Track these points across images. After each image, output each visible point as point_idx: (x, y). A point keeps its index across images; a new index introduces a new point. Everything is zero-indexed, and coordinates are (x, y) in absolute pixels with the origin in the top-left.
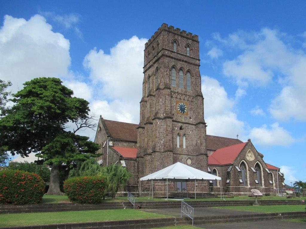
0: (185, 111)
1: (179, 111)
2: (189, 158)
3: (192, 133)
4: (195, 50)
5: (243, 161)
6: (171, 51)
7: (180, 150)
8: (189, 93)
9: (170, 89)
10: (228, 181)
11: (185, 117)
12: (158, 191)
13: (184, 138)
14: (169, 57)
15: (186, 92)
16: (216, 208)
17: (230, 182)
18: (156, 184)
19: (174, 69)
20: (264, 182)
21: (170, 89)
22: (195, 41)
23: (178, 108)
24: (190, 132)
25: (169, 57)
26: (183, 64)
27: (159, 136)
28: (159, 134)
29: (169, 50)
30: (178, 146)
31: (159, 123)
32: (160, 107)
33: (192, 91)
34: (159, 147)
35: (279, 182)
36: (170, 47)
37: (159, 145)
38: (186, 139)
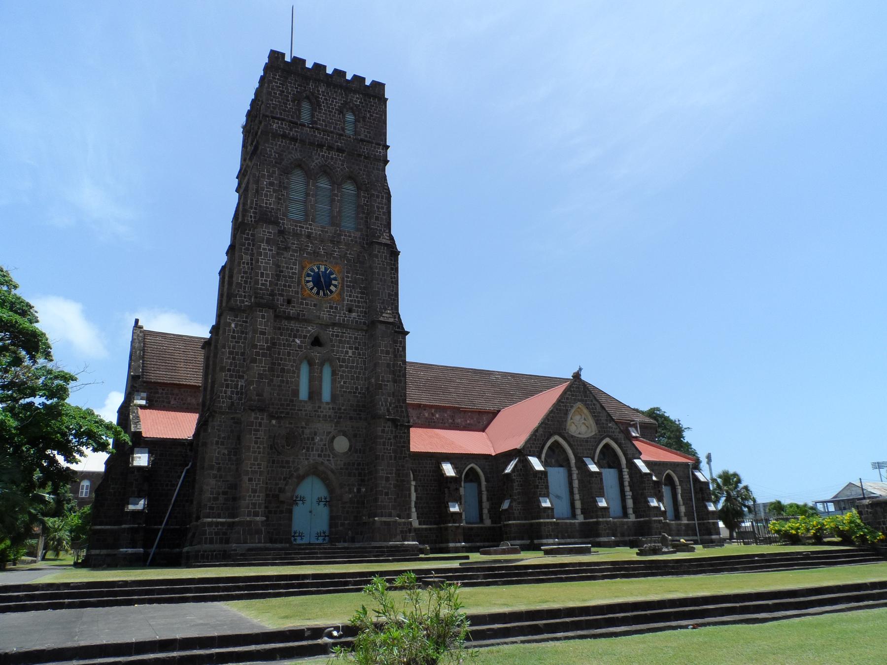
0: (332, 288)
1: (312, 289)
3: (354, 353)
4: (374, 120)
5: (557, 438)
8: (350, 236)
9: (276, 223)
10: (506, 505)
11: (331, 307)
12: (211, 542)
13: (327, 372)
14: (284, 136)
15: (340, 235)
17: (510, 506)
18: (210, 520)
19: (298, 172)
20: (634, 503)
21: (276, 223)
22: (375, 97)
23: (308, 282)
24: (347, 352)
25: (284, 136)
26: (332, 158)
28: (234, 359)
30: (304, 394)
31: (233, 326)
32: (242, 277)
33: (358, 234)
35: (697, 499)
36: (289, 111)
37: (229, 393)
38: (334, 373)
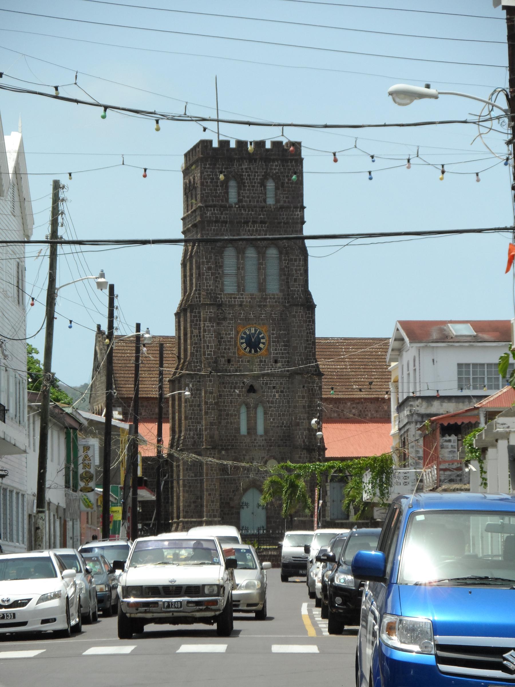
0: (261, 346)
1: (245, 349)
2: (271, 456)
3: (280, 396)
6: (221, 206)
7: (248, 441)
13: (260, 412)
16: (103, 365)
23: (242, 343)
24: (275, 396)
27: (192, 413)
29: (214, 206)
30: (243, 430)
34: (193, 438)
36: (219, 196)
